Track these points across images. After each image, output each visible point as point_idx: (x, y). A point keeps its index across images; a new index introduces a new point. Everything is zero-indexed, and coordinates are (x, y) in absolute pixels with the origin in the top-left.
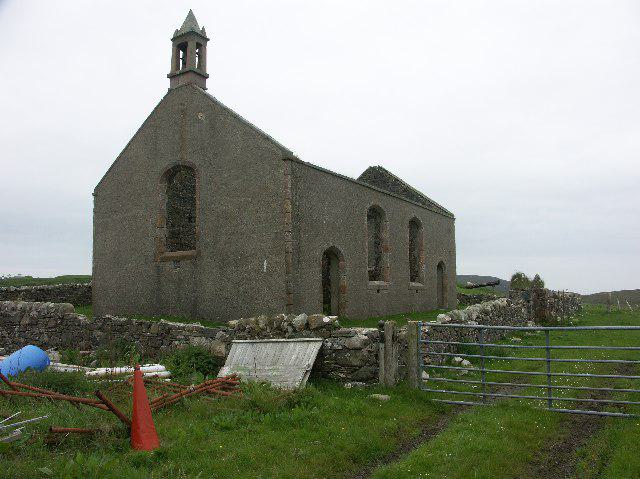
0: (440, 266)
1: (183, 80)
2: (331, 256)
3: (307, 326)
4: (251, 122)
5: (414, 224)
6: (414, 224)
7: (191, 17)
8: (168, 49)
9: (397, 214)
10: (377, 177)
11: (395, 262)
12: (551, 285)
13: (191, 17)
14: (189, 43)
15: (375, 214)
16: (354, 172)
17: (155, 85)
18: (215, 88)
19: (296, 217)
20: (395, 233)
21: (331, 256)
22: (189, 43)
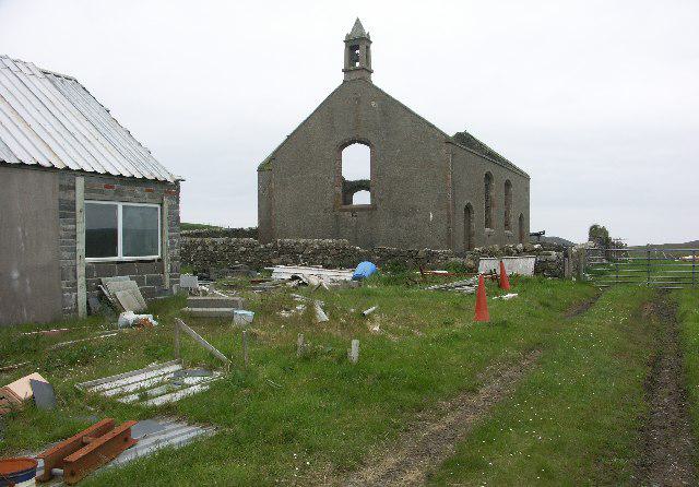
0: (521, 218)
1: (354, 76)
2: (468, 209)
3: (525, 250)
4: (524, 170)
5: (508, 184)
6: (508, 184)
7: (358, 23)
8: (341, 49)
9: (500, 177)
10: (464, 139)
11: (497, 214)
12: (613, 235)
13: (358, 23)
14: (357, 46)
15: (488, 177)
16: (451, 134)
17: (331, 76)
18: (377, 79)
19: (453, 183)
20: (497, 192)
21: (468, 209)
22: (357, 46)
